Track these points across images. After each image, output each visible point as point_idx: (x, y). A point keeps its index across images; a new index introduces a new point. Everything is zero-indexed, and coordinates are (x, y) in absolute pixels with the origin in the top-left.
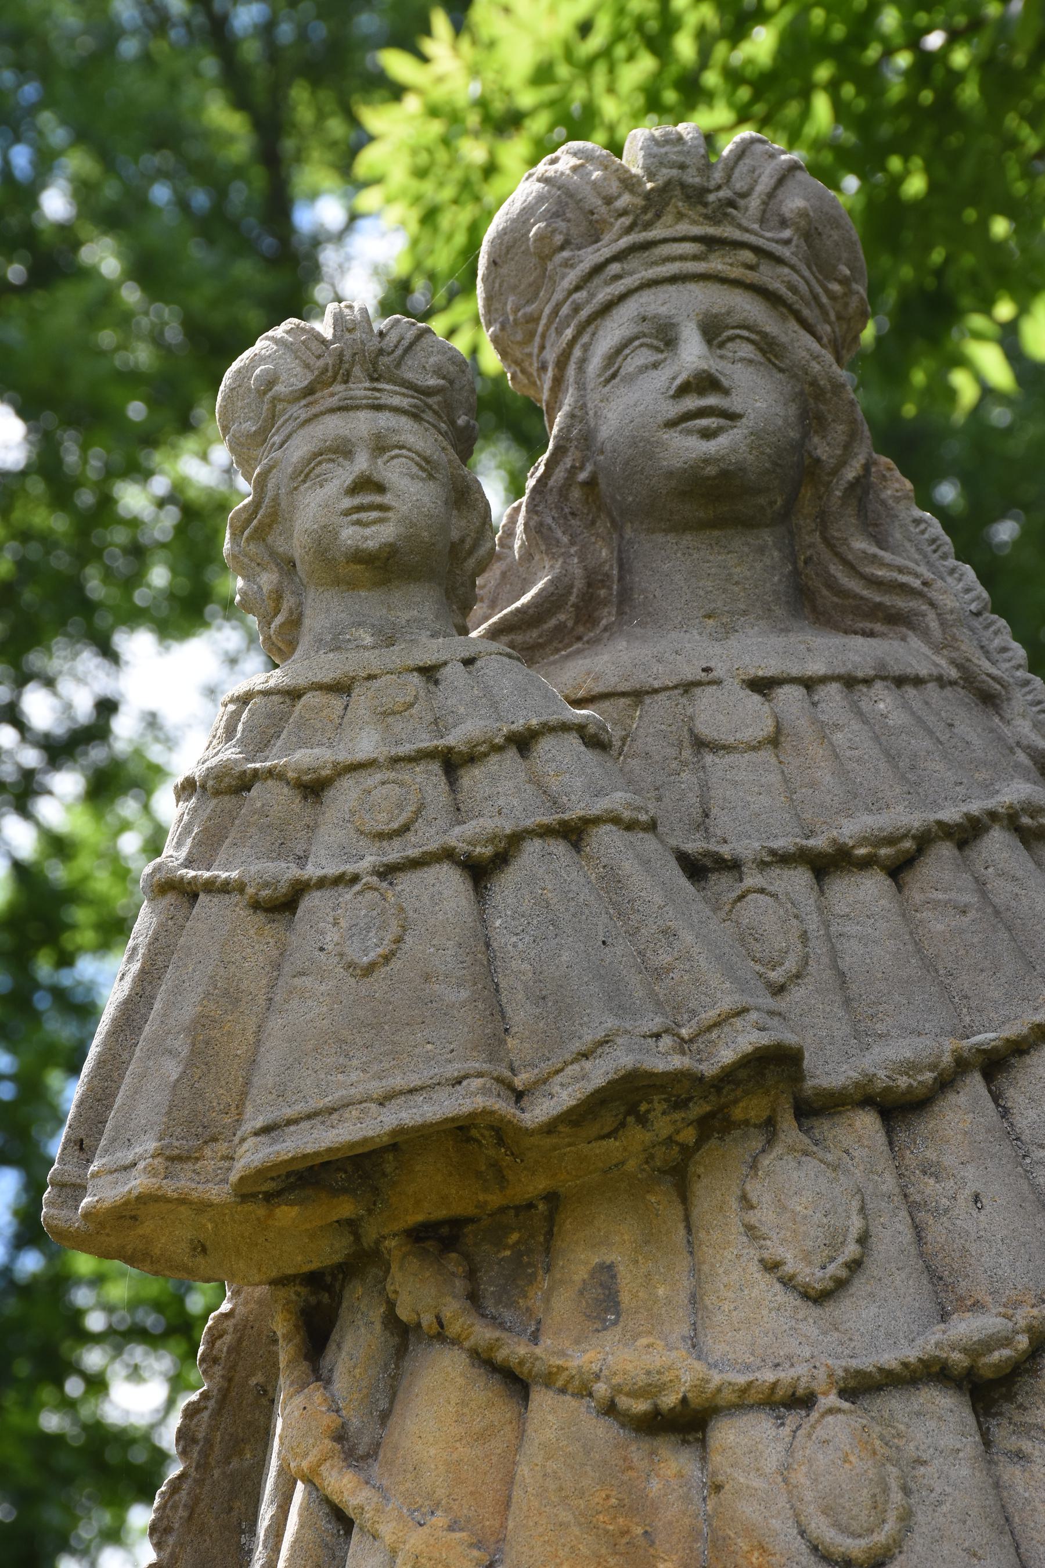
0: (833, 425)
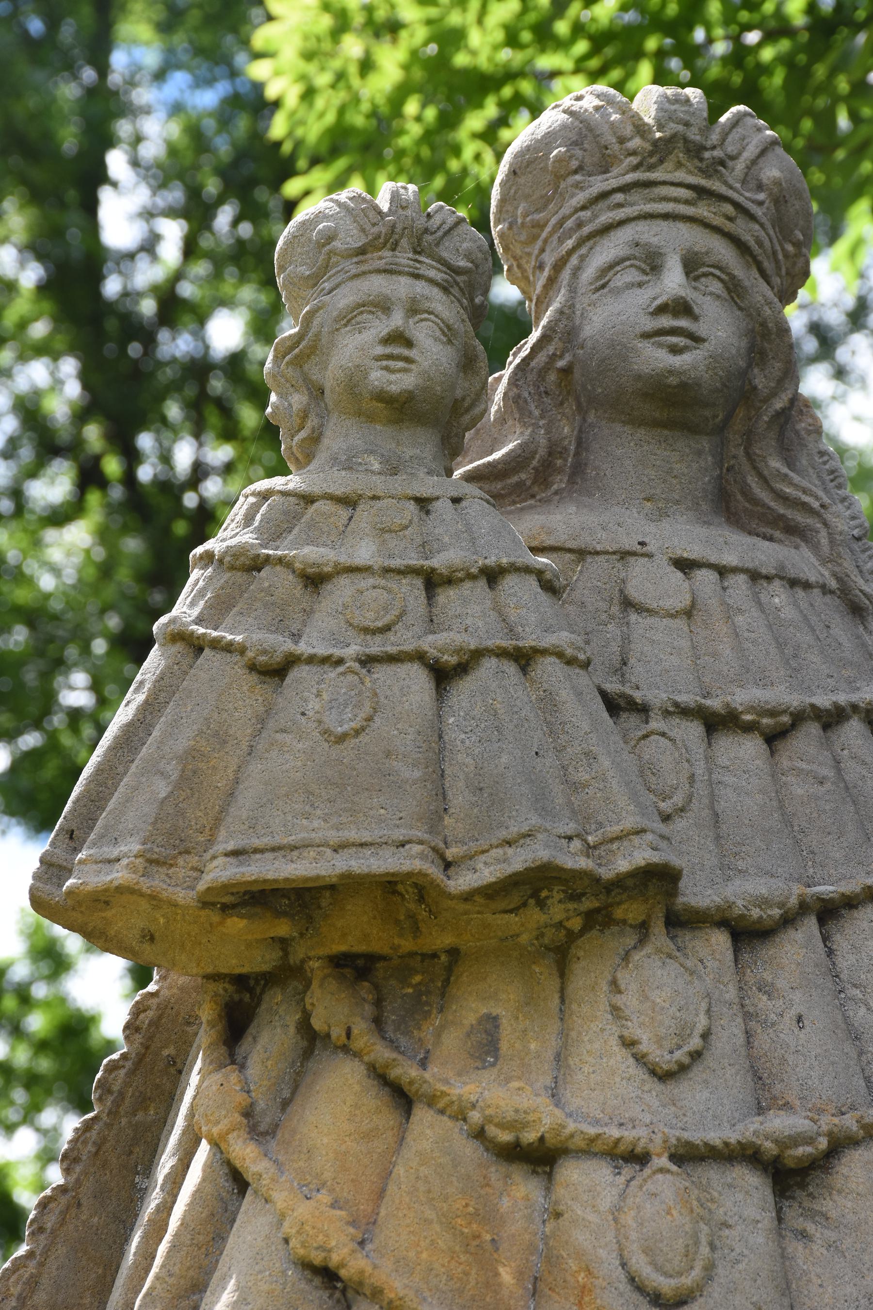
0: (771, 361)
